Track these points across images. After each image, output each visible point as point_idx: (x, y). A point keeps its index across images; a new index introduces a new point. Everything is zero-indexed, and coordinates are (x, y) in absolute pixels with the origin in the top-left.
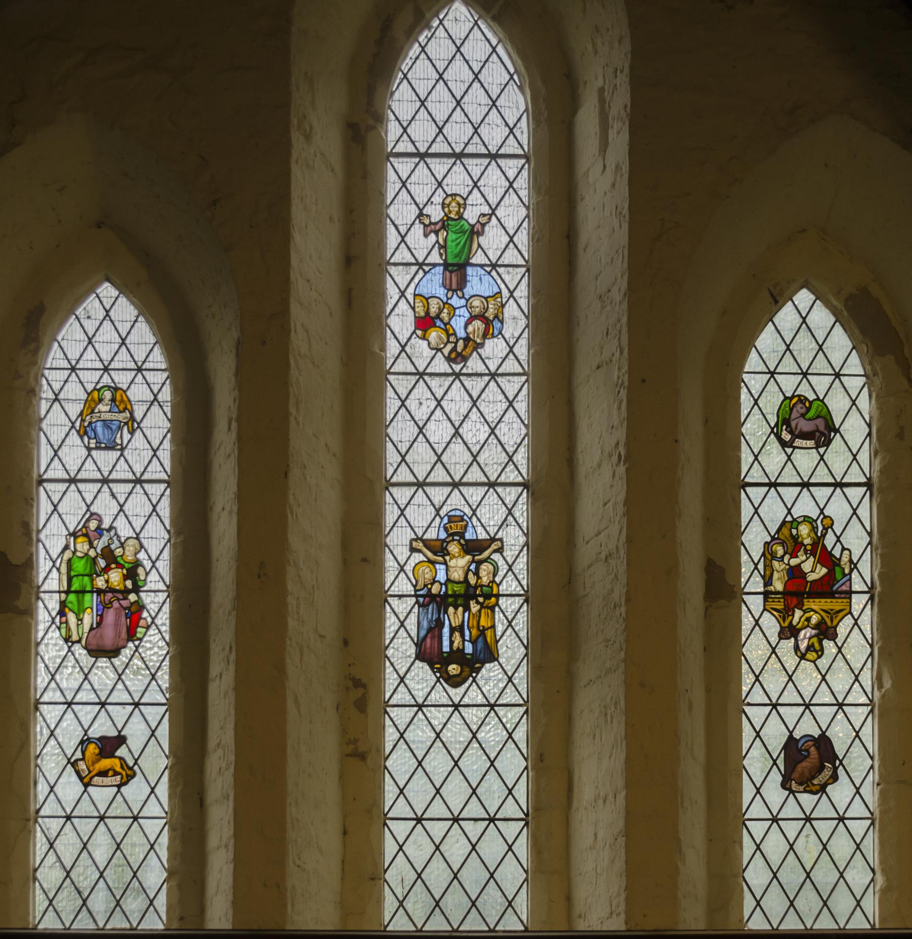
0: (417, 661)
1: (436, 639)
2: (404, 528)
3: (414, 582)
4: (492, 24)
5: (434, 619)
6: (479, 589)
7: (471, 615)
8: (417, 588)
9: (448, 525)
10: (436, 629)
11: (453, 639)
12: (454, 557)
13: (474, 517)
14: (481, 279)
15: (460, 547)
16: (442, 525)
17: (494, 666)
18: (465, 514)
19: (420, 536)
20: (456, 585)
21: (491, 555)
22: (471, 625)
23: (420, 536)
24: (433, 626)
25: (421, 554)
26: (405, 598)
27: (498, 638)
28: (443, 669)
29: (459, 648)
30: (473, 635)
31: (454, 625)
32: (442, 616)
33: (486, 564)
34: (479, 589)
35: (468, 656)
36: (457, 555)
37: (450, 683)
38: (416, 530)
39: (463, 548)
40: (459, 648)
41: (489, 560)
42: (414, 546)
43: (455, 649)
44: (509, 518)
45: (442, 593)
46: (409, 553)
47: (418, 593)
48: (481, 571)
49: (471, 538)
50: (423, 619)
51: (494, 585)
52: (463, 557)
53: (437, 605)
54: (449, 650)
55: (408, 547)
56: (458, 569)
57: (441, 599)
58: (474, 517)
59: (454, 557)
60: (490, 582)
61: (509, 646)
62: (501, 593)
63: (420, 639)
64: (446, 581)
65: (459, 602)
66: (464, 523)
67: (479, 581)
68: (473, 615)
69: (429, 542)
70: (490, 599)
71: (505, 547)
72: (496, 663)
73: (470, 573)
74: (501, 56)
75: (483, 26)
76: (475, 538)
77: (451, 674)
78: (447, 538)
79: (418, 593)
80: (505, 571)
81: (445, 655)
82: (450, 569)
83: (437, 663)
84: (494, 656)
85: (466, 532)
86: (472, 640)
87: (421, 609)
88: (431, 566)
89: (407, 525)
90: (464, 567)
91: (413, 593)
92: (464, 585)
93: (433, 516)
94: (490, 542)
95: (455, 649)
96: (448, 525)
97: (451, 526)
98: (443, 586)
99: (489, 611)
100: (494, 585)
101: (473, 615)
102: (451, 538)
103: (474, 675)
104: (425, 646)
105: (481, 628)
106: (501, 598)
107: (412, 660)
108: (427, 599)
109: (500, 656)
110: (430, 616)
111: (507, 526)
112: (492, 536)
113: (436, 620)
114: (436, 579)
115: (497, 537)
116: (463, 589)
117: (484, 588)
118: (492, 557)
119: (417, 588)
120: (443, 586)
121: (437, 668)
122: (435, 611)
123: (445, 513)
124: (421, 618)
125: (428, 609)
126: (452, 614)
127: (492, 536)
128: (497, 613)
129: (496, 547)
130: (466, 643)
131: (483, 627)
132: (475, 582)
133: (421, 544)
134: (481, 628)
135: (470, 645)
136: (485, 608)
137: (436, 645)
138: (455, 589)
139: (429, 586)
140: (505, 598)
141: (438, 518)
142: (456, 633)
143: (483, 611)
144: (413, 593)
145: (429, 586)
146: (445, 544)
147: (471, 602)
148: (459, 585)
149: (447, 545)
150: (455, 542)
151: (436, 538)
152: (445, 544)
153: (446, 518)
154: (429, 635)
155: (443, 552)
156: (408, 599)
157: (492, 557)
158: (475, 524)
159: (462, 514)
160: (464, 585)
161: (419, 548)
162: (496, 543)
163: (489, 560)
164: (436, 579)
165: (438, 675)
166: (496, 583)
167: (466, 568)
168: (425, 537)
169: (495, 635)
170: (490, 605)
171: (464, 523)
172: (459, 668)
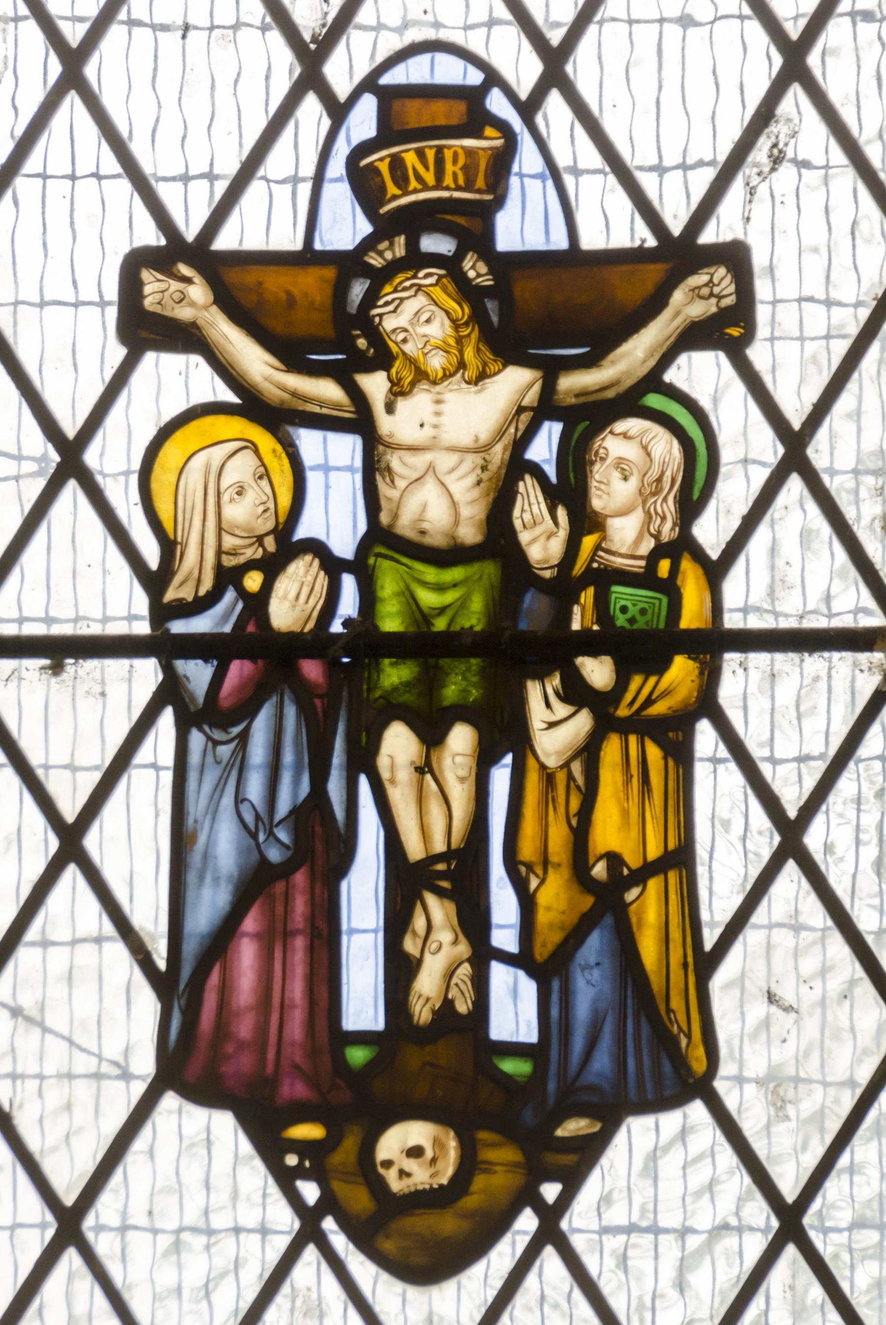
0: (170, 1101)
1: (300, 943)
2: (87, 188)
3: (151, 553)
4: (182, 895)
5: (283, 807)
6: (588, 596)
7: (533, 782)
8: (170, 595)
9: (380, 159)
10: (300, 878)
11: (410, 946)
12: (421, 375)
13: (555, 101)
14: (724, 910)
15: (461, 312)
16: (341, 151)
17: (683, 1134)
18: (493, 78)
19: (190, 232)
20: (430, 573)
21: (667, 359)
22: (527, 850)
23: (190, 234)
24: (274, 855)
25: (197, 360)
26: (91, 666)
27: (710, 938)
28: (350, 1145)
29: (448, 1004)
30: (543, 917)
31: (415, 850)
32: (335, 788)
33: (633, 425)
34: (588, 596)
35: (511, 1066)
36: (436, 362)
37: (388, 1246)
38: (168, 193)
39: (479, 317)
40: (448, 1004)
41: (654, 401)
42: (149, 303)
43: (422, 1013)
44: (786, 106)
45: (337, 627)
46: (118, 353)
47: (178, 627)
48: (598, 472)
49: (535, 241)
50: (214, 811)
51: (687, 565)
52: (482, 376)
53: (305, 711)
54: (380, 1025)
55: (112, 313)
56: (445, 461)
57: (333, 666)
58: (555, 101)
59: (421, 375)
60: (660, 551)
61: (787, 993)
62: (732, 621)
63: (190, 949)
64: (365, 546)
65: (451, 692)
66: (492, 140)
67: (588, 542)
68: (548, 777)
69: (251, 276)
70: (661, 666)
71: (762, 314)
72: (697, 1110)
73: (528, 487)
74: (14, 46)
75: (339, 1241)
76: (560, 241)
77: (396, 1185)
78: (368, 244)
79: (178, 627)
80: (760, 476)
81: (358, 1056)
82: (395, 461)
83: (303, 1114)
84: (680, 1062)
85: (500, 201)
86: (541, 952)
87: (196, 739)
88: (265, 441)
89: (111, 164)
90: (483, 449)
91: (143, 628)
92: (489, 570)
93: (281, 87)
94: (655, 272)
95: (422, 1013)
96: (380, 159)
97: (397, 163)
98: (349, 583)
99: (654, 752)
100: (687, 565)
101: (548, 777)
102: (400, 245)
103: (551, 1191)
104: (226, 989)
105: (599, 870)
106: (731, 659)
107: (139, 1089)
108: (238, 670)
109: (726, 1068)
110: (255, 788)
111: (777, 160)
112: (676, 228)
113: (296, 812)
114: (302, 532)
115: (708, 237)
116: (477, 604)
117: (621, 594)
118: (670, 376)
119: (170, 595)
120: (349, 583)
121: (303, 1147)
122: (288, 757)
123: (362, 70)
124: (196, 804)
125: (244, 738)
126: (405, 775)
127: (676, 228)
128: (701, 772)
129: (699, 310)
130: (500, 974)
131: (614, 859)
132: (556, 547)
133: (199, 292)
134: (599, 870)
135: (529, 988)
136: (625, 727)
137: (297, 990)
138: (428, 598)
139: (253, 581)
140: (759, 660)
141: (311, 106)
142: (431, 900)
143: (611, 749)
144: (143, 628)
145: (253, 581)
146: (358, 290)
147: (534, 691)
148: (456, 573)
149: (371, 298)
150: (428, 276)
151: (297, 245)
152: (358, 290)
153: (368, 105)
154: (250, 923)
155: (344, 344)
156: (116, 667)
157: (670, 376)
158: (562, 160)
159: (475, 77)
160: (489, 570)
161: (184, 314)
162: (698, 279)
163: (654, 401)
164: (302, 532)
165: (310, 1192)
166: (699, 555)
167: (499, 454)
168: (224, 241)
169: (695, 926)
170: (659, 708)
171: (492, 140)
172: (452, 1144)
